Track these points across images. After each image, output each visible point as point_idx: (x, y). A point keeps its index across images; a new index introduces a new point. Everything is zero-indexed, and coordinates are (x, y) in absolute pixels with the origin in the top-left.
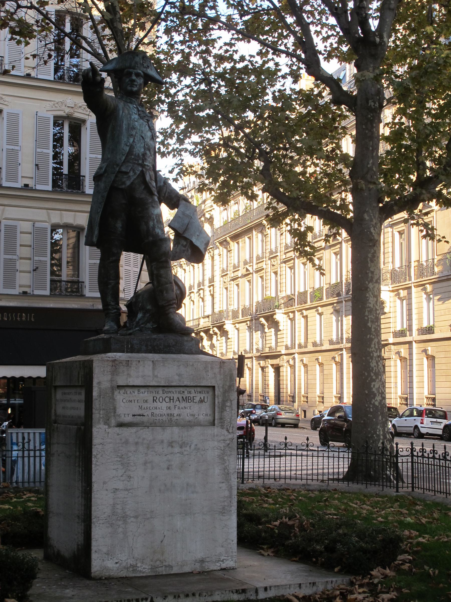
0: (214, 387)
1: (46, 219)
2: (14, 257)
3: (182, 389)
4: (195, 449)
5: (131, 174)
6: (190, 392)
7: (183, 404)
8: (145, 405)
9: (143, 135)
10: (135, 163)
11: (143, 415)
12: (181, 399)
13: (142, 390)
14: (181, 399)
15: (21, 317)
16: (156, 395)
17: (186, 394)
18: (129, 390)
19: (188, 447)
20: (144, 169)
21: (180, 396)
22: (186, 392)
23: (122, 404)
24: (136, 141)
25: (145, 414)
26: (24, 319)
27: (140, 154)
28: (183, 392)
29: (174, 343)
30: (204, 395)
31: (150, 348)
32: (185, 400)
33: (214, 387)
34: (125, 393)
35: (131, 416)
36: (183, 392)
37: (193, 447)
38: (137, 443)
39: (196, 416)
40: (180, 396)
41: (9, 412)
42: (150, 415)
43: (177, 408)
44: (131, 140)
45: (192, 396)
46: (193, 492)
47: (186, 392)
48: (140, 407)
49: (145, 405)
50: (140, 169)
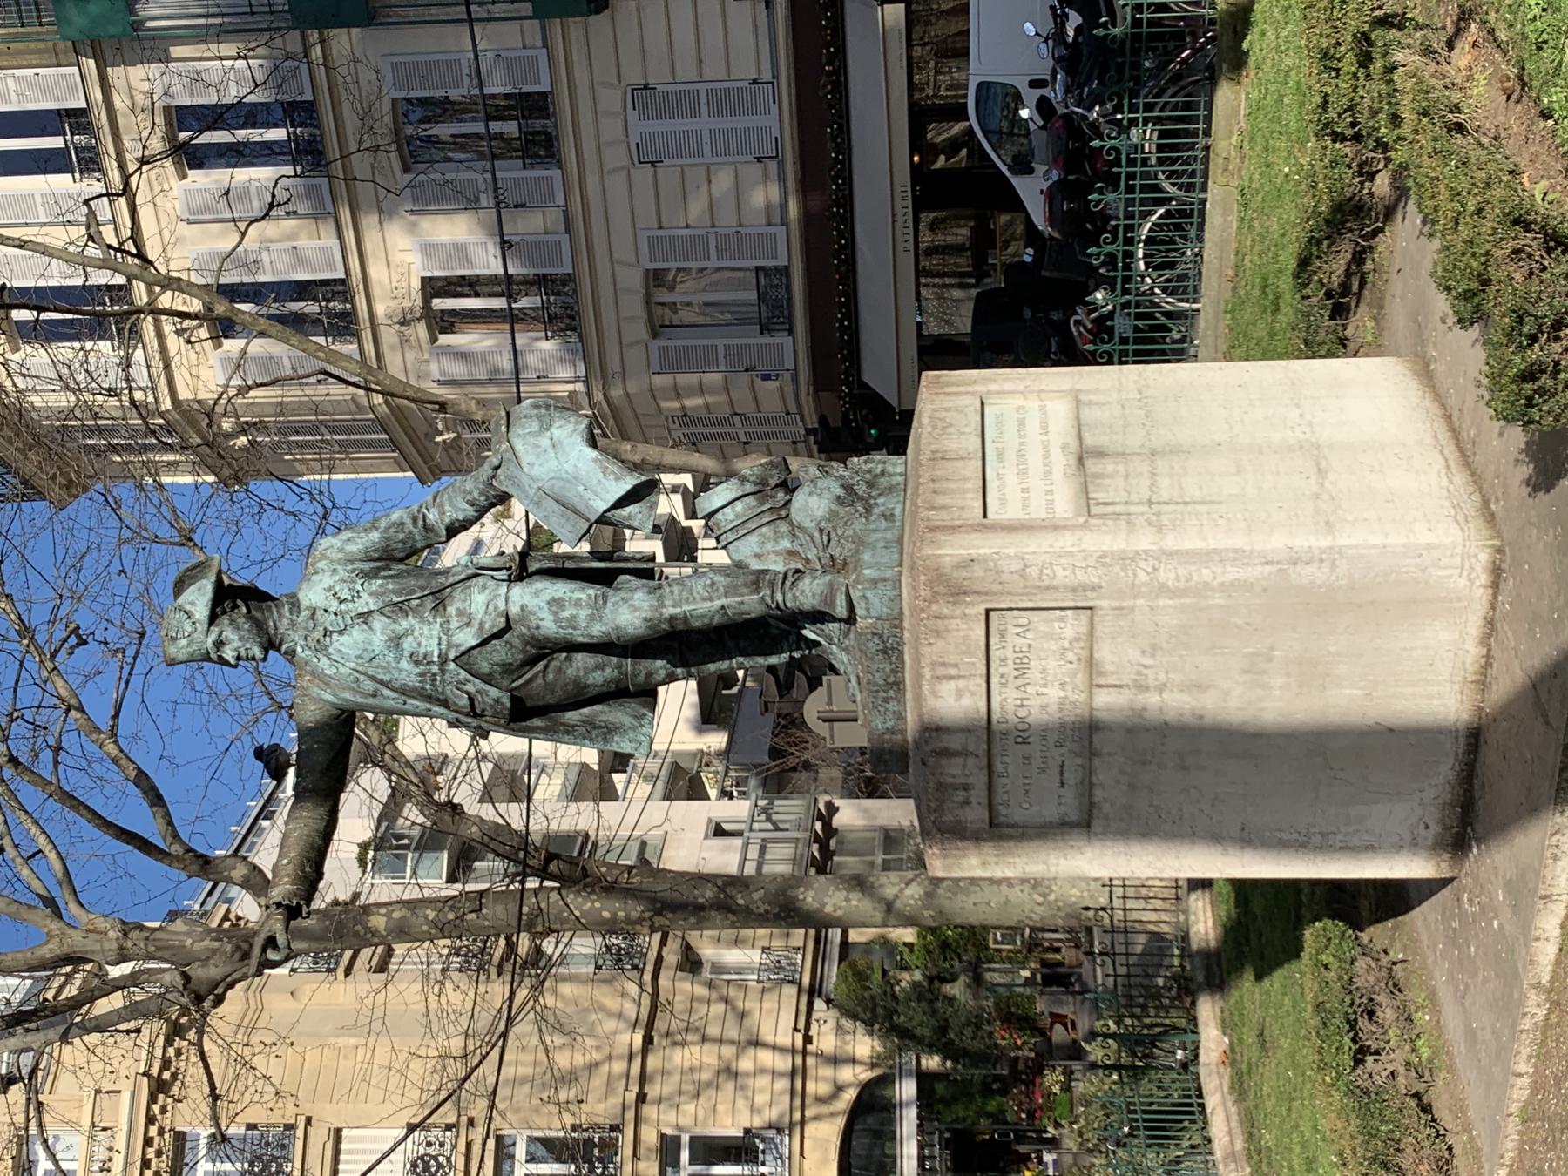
1: (624, 173)
2: (712, 239)
3: (994, 681)
4: (1153, 656)
5: (470, 688)
6: (1003, 660)
7: (1034, 675)
8: (1037, 762)
9: (367, 656)
10: (443, 681)
11: (1062, 766)
12: (1020, 682)
13: (999, 767)
14: (1020, 682)
16: (1011, 738)
17: (1009, 669)
18: (1000, 797)
19: (1146, 672)
20: (452, 655)
21: (1013, 684)
22: (1002, 670)
23: (1035, 808)
24: (386, 678)
25: (1059, 760)
27: (417, 671)
28: (1002, 676)
29: (876, 640)
30: (1010, 627)
31: (891, 693)
32: (1021, 671)
34: (1007, 804)
35: (1062, 792)
36: (1002, 676)
37: (1148, 661)
39: (1066, 644)
40: (1013, 684)
41: (1028, 25)
42: (1063, 750)
43: (1044, 691)
44: (387, 692)
45: (1011, 655)
46: (1270, 660)
47: (1002, 670)
48: (1042, 771)
49: (1037, 762)
50: (452, 666)
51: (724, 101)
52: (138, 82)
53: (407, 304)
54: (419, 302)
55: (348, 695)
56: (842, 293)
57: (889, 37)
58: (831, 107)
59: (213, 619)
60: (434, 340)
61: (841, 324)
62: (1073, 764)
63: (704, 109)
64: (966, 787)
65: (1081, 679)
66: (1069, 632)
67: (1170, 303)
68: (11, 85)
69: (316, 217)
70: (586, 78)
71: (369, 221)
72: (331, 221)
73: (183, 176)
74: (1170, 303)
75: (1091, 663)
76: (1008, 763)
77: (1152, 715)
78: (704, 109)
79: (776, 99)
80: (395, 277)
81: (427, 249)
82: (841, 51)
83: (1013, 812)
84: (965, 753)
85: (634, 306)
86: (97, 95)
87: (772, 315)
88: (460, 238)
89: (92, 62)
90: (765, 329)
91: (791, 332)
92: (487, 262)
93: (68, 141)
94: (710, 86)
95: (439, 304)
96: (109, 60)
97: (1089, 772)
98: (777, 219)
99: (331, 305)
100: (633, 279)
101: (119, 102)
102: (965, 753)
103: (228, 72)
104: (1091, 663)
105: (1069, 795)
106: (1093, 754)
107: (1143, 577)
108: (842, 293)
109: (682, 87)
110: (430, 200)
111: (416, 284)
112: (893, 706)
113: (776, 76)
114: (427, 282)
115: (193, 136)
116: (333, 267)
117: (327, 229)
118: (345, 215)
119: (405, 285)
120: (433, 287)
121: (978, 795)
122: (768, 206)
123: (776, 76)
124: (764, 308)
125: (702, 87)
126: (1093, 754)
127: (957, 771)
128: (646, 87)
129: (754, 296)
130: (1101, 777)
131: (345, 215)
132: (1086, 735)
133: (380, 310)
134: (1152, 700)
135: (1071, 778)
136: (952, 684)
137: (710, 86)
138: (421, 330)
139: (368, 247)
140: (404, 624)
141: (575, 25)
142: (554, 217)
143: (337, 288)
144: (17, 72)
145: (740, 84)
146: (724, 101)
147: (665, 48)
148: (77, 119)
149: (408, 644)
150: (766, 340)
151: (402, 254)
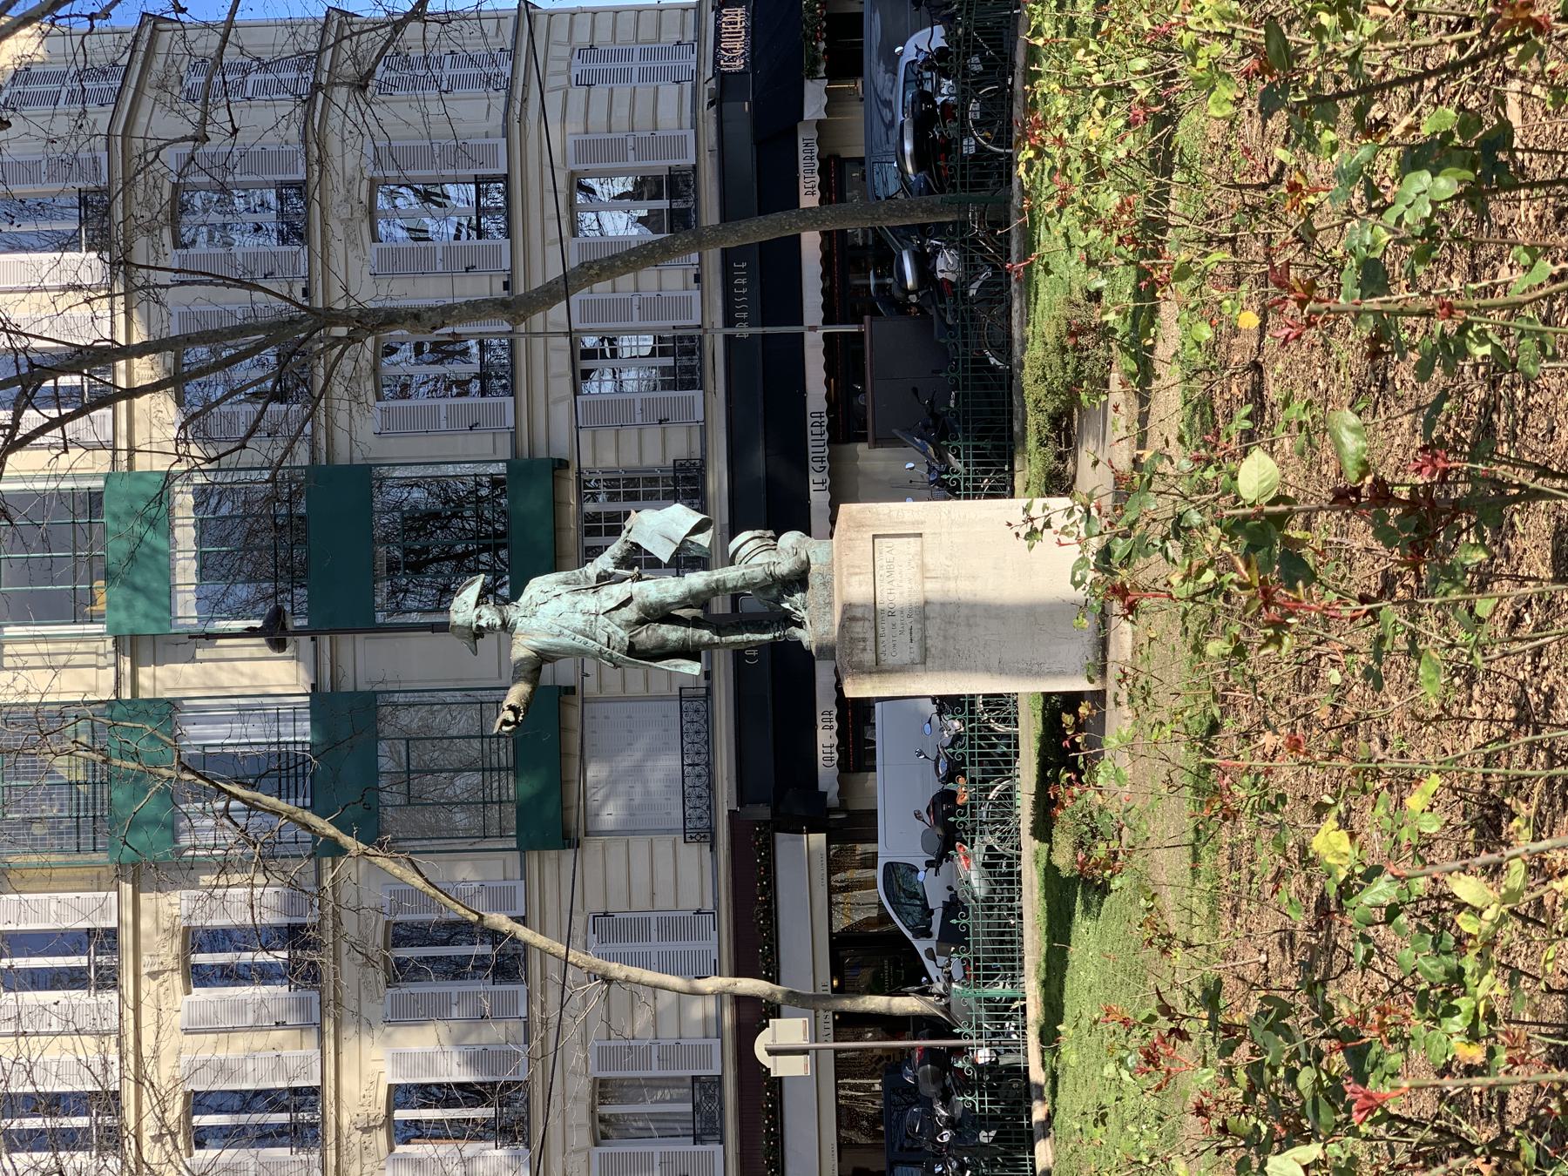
0: (875, 536)
2: (655, 1048)
5: (609, 630)
7: (896, 575)
13: (880, 631)
15: (740, 287)
26: (745, 315)
33: (875, 536)
38: (945, 638)
49: (899, 626)
51: (672, 927)
52: (171, 907)
53: (373, 1111)
54: (383, 1111)
55: (544, 639)
56: (770, 1100)
57: (813, 861)
58: (762, 930)
59: (477, 605)
60: (391, 1150)
61: (768, 1130)
62: (916, 627)
63: (654, 934)
64: (864, 640)
65: (918, 576)
66: (912, 551)
67: (1001, 728)
68: (53, 906)
69: (302, 1028)
70: (555, 907)
71: (348, 1032)
72: (315, 1031)
73: (188, 993)
74: (1001, 728)
75: (923, 567)
76: (885, 627)
77: (953, 596)
78: (654, 934)
79: (716, 926)
80: (365, 1085)
81: (398, 1058)
82: (772, 886)
83: (889, 659)
84: (863, 619)
85: (579, 1115)
86: (128, 916)
87: (705, 1129)
88: (431, 1051)
89: (129, 886)
90: (697, 1139)
91: (721, 1142)
92: (454, 1071)
93: (91, 960)
94: (660, 914)
95: (401, 1115)
96: (143, 887)
97: (924, 630)
98: (713, 1031)
99: (300, 1115)
100: (581, 1087)
101: (146, 924)
102: (863, 619)
103: (250, 900)
104: (923, 567)
105: (915, 646)
106: (926, 618)
107: (944, 517)
108: (770, 1100)
109: (637, 915)
110: (404, 1016)
111: (382, 1093)
112: (828, 617)
113: (717, 906)
114: (393, 1089)
115: (209, 957)
116: (308, 1075)
117: (311, 1039)
118: (329, 1027)
119: (372, 1093)
120: (400, 1095)
121: (870, 644)
122: (706, 1019)
123: (717, 906)
124: (697, 1118)
125: (653, 916)
126: (926, 618)
127: (859, 630)
128: (605, 914)
129: (689, 1107)
130: (930, 632)
131: (329, 1027)
132: (923, 612)
133: (345, 1120)
134: (951, 585)
135: (916, 637)
136: (857, 578)
137: (660, 914)
138: (382, 1136)
139: (344, 1058)
140: (578, 598)
141: (553, 854)
142: (516, 1027)
143: (307, 1097)
144: (61, 896)
145: (685, 914)
146: (672, 927)
147: (624, 882)
148: (108, 939)
149: (579, 606)
150: (699, 1148)
151: (375, 1064)
